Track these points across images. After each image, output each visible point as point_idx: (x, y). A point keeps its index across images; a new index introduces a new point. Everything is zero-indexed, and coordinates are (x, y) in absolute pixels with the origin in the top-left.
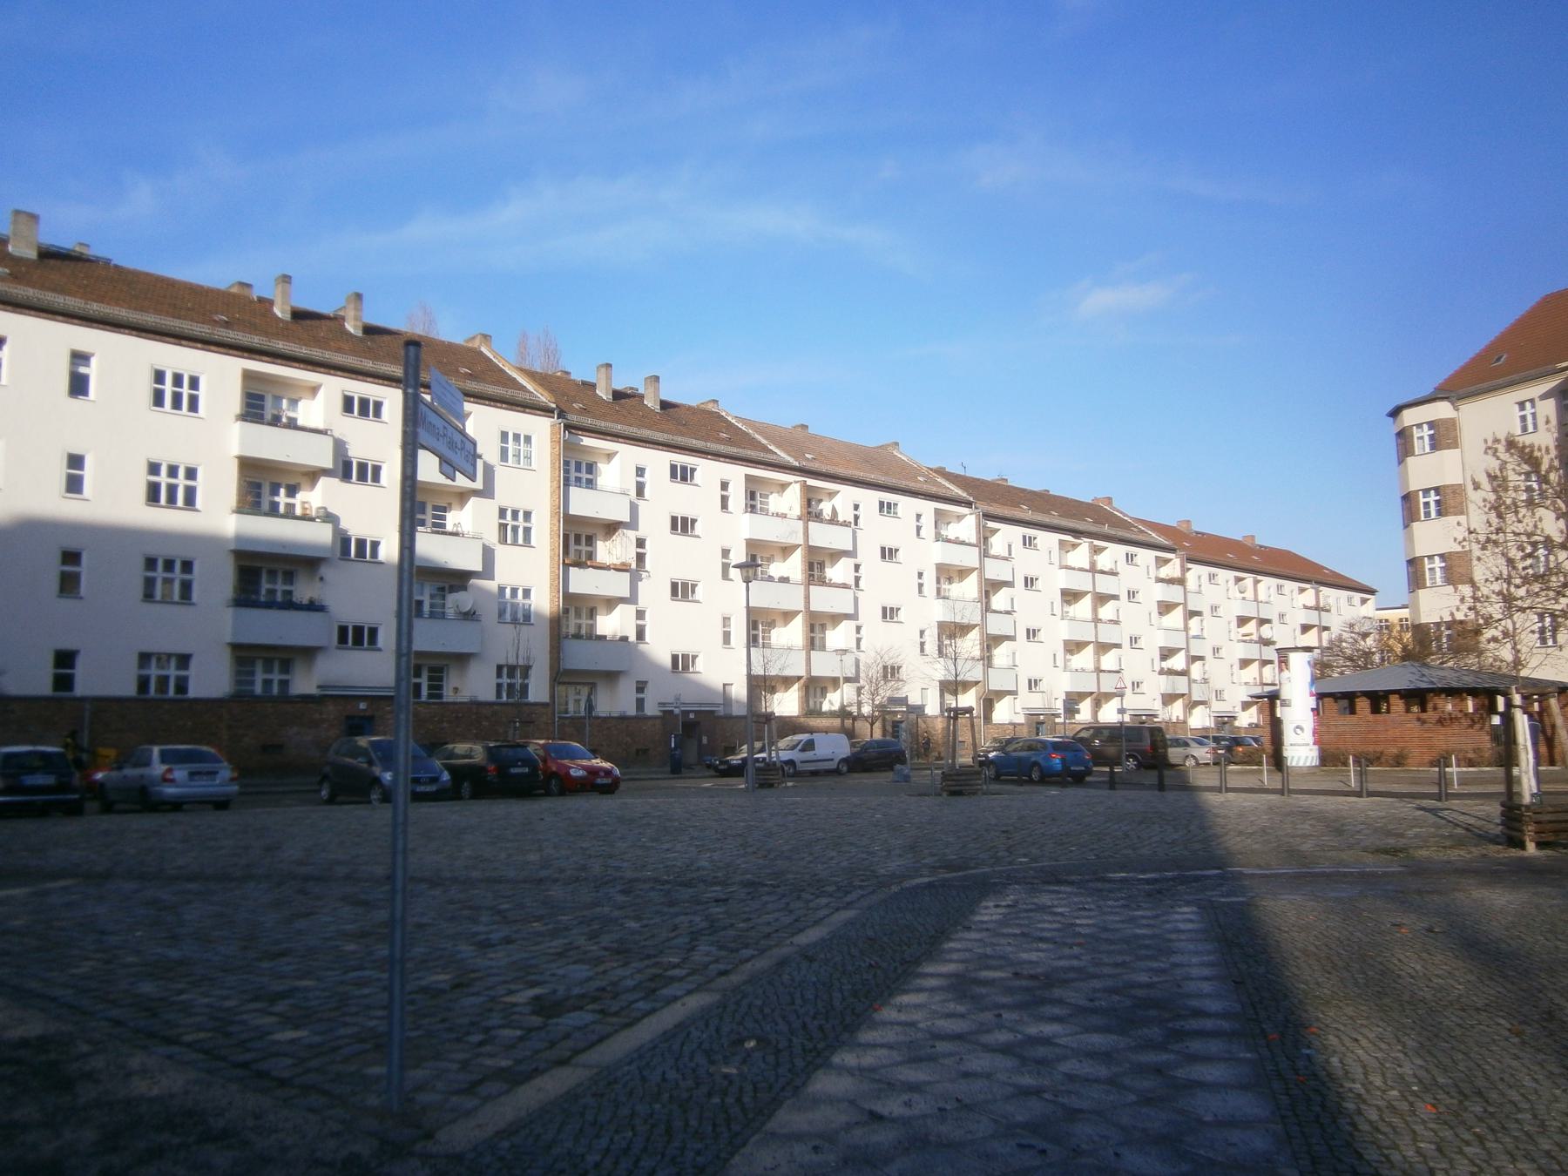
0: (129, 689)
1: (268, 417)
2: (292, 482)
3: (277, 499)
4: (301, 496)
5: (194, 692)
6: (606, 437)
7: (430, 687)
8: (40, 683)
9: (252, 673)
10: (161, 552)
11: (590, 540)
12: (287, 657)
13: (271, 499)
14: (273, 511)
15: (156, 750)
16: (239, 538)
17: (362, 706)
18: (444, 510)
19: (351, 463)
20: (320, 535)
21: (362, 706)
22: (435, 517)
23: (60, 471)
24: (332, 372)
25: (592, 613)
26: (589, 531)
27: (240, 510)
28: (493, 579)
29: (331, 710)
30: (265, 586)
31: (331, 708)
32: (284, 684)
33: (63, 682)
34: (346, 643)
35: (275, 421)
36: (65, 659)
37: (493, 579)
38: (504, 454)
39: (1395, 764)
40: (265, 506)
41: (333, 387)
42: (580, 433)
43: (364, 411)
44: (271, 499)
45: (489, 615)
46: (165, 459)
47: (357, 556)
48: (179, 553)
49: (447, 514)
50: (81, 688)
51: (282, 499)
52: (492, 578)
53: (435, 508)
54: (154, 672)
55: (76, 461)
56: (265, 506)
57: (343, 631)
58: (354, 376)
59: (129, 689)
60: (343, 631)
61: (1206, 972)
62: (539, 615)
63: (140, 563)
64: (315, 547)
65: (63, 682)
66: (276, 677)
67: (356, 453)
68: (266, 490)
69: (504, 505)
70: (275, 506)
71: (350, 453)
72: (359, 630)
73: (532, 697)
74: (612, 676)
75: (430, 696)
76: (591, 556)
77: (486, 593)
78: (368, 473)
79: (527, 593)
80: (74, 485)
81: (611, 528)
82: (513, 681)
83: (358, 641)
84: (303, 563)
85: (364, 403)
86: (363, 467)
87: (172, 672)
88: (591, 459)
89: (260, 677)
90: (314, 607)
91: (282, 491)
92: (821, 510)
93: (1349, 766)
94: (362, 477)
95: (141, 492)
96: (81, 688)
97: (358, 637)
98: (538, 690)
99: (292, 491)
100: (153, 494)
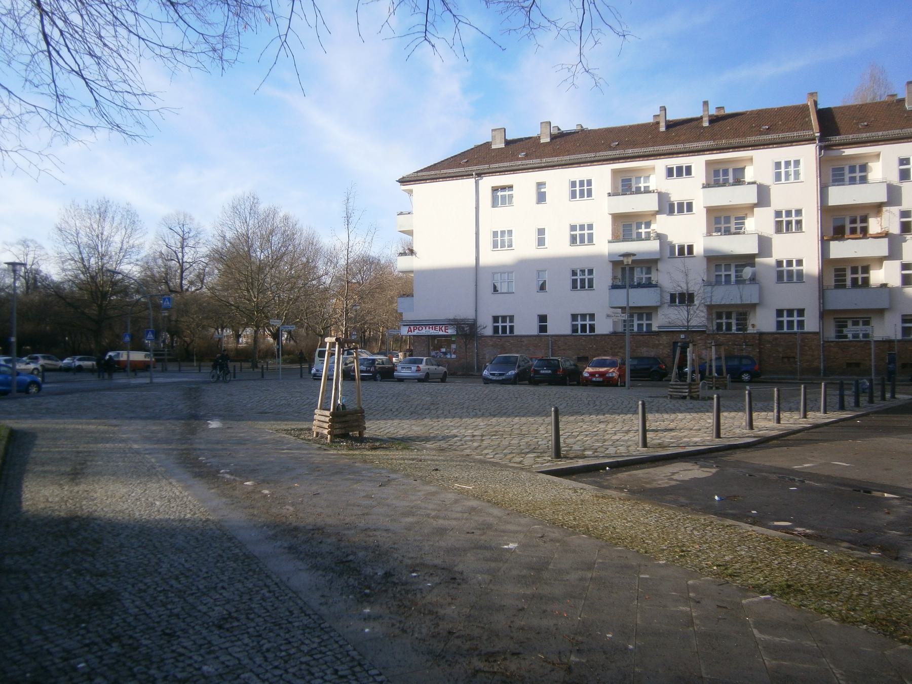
0: (567, 331)
1: (634, 189)
2: (648, 220)
3: (640, 231)
4: (653, 226)
6: (866, 145)
7: (737, 325)
8: (534, 330)
10: (578, 267)
11: (865, 219)
12: (647, 312)
13: (637, 231)
14: (639, 238)
16: (610, 255)
17: (682, 336)
18: (743, 218)
19: (674, 204)
20: (653, 246)
21: (682, 336)
22: (736, 224)
23: (534, 237)
24: (658, 157)
25: (866, 270)
26: (863, 213)
27: (709, 233)
28: (772, 257)
29: (664, 339)
31: (665, 338)
32: (649, 326)
33: (543, 329)
35: (638, 191)
36: (543, 319)
37: (772, 257)
38: (778, 177)
40: (634, 236)
41: (661, 165)
42: (841, 147)
43: (680, 174)
44: (637, 231)
46: (577, 222)
47: (688, 254)
48: (586, 266)
49: (745, 221)
50: (550, 331)
51: (643, 230)
53: (737, 218)
54: (579, 322)
55: (541, 232)
56: (634, 236)
58: (671, 156)
59: (567, 331)
62: (810, 277)
63: (569, 274)
64: (650, 253)
65: (543, 329)
66: (645, 322)
67: (675, 198)
68: (634, 227)
69: (779, 208)
70: (639, 234)
71: (672, 199)
74: (880, 312)
75: (738, 330)
77: (767, 266)
79: (800, 262)
80: (541, 242)
81: (877, 208)
84: (649, 263)
85: (680, 169)
86: (681, 205)
87: (795, 318)
88: (862, 162)
90: (649, 285)
91: (643, 226)
92: (286, 218)
94: (681, 211)
95: (568, 239)
96: (550, 331)
97: (685, 299)
98: (812, 324)
99: (648, 225)
100: (573, 240)
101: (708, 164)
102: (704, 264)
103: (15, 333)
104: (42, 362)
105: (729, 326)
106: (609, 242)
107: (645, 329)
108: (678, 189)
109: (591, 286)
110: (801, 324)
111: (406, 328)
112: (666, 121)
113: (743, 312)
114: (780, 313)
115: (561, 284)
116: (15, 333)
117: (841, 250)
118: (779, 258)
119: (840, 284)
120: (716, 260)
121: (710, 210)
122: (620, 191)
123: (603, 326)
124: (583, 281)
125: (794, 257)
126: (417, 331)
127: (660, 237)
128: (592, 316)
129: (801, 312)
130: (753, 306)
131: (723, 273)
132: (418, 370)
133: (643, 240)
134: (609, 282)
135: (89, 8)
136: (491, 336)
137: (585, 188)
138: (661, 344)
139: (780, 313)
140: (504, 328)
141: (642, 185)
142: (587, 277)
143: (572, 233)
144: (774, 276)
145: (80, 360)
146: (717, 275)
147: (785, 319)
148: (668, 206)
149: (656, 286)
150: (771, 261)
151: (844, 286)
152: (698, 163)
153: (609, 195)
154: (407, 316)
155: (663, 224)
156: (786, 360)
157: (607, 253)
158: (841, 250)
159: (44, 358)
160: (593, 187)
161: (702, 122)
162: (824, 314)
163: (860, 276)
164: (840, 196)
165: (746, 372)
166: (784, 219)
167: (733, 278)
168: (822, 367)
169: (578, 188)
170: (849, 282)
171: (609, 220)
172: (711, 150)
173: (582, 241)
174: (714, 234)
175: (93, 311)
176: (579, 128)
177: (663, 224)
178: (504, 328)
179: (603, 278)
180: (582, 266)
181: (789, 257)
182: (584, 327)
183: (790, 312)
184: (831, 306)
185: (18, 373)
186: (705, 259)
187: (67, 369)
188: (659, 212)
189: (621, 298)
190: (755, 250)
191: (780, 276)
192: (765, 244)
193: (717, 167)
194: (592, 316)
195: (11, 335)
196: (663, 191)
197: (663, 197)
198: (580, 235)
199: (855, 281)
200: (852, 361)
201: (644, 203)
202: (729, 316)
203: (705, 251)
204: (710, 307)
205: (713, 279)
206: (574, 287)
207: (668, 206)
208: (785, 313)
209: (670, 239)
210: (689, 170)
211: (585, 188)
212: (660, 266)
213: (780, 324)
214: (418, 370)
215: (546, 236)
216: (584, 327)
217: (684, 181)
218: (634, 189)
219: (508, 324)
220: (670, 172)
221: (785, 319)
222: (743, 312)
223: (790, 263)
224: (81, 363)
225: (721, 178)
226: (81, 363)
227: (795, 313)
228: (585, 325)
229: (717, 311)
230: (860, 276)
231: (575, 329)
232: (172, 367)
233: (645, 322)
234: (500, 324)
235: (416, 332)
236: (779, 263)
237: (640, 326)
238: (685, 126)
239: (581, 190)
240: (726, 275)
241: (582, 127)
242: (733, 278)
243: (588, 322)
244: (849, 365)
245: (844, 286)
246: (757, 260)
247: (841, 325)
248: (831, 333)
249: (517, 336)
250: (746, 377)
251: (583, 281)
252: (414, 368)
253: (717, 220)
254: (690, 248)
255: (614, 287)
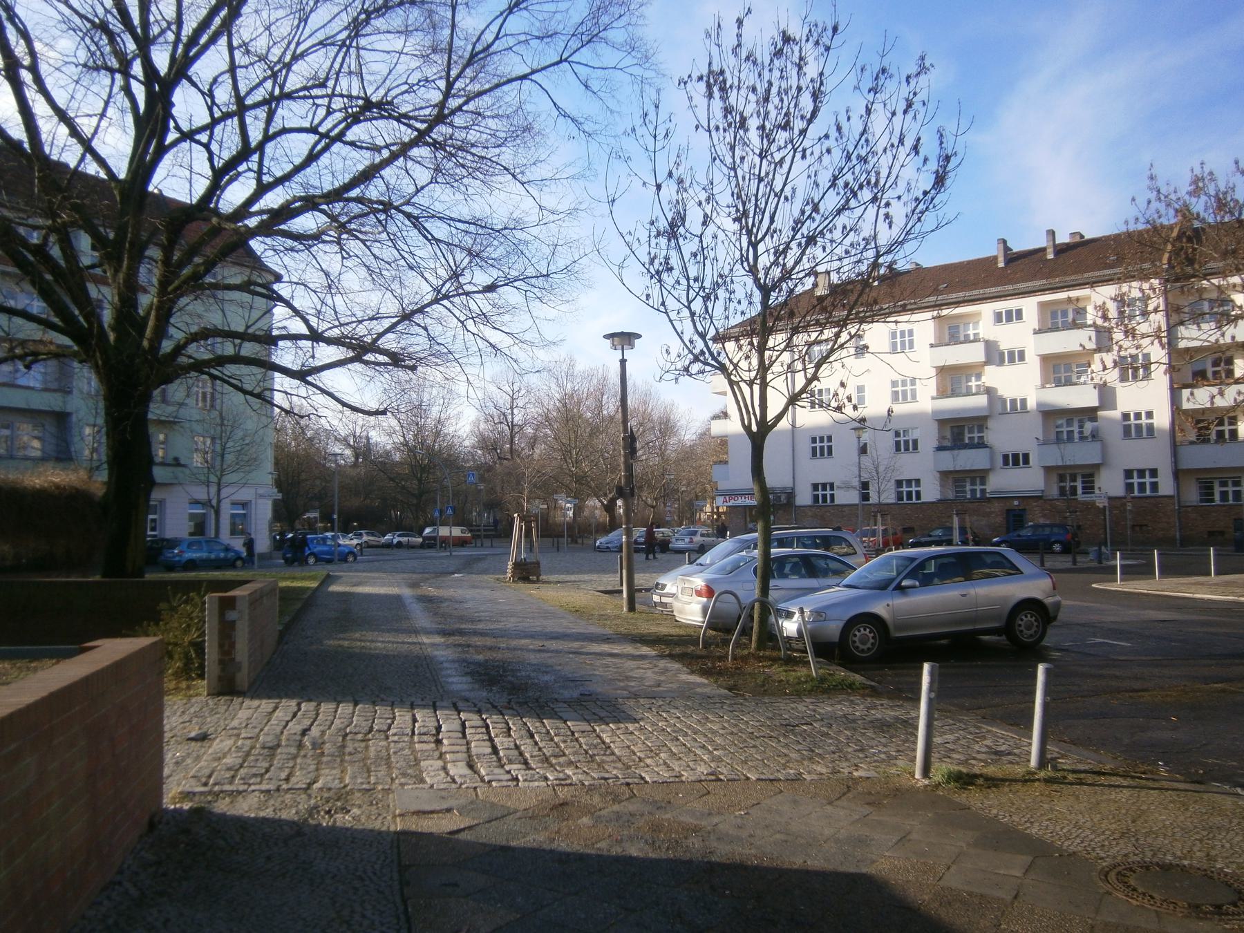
1: (962, 338)
4: (984, 379)
5: (837, 502)
7: (1084, 488)
9: (965, 487)
10: (817, 435)
11: (1230, 361)
12: (981, 476)
15: (150, 533)
16: (934, 412)
17: (1016, 503)
21: (1016, 503)
29: (997, 507)
30: (967, 435)
33: (865, 497)
34: (1008, 464)
35: (967, 340)
39: (813, 559)
41: (987, 310)
43: (1009, 319)
45: (1114, 437)
48: (825, 434)
51: (973, 383)
52: (1113, 407)
54: (905, 489)
57: (1006, 457)
60: (1006, 457)
61: (450, 680)
62: (1161, 431)
65: (865, 497)
66: (978, 488)
67: (1005, 346)
70: (969, 388)
72: (1016, 456)
73: (926, 498)
76: (1230, 373)
77: (1111, 421)
78: (1017, 356)
79: (1150, 415)
82: (974, 487)
83: (1016, 463)
84: (979, 421)
85: (1009, 313)
86: (1011, 354)
87: (1148, 480)
89: (968, 487)
90: (981, 445)
93: (1122, 566)
94: (1012, 360)
96: (837, 502)
97: (1017, 460)
98: (1166, 486)
99: (979, 377)
101: (1043, 306)
102: (1039, 420)
103: (336, 511)
104: (365, 538)
105: (1074, 489)
106: (933, 398)
107: (978, 496)
108: (1009, 337)
109: (830, 453)
110: (1154, 486)
111: (722, 499)
112: (1055, 246)
113: (1089, 475)
114: (1128, 474)
115: (882, 445)
116: (336, 511)
117: (1200, 398)
118: (1126, 410)
119: (1203, 439)
120: (1050, 414)
121: (1046, 359)
122: (947, 340)
123: (931, 492)
124: (822, 448)
125: (1143, 408)
126: (732, 501)
127: (989, 391)
128: (918, 482)
129: (1154, 472)
130: (1097, 467)
131: (1065, 429)
132: (691, 542)
133: (973, 395)
134: (935, 444)
135: (473, 150)
136: (810, 506)
137: (907, 339)
138: (993, 512)
139: (1128, 474)
140: (824, 497)
141: (971, 332)
142: (826, 444)
143: (894, 389)
144: (1120, 431)
145: (399, 536)
146: (1057, 432)
147: (1136, 480)
148: (994, 355)
149: (986, 446)
150: (1116, 414)
151: (1208, 441)
152: (1029, 305)
153: (932, 346)
154: (722, 485)
155: (993, 377)
156: (1137, 528)
157: (930, 411)
158: (1200, 398)
159: (367, 534)
160: (915, 338)
161: (1046, 255)
162: (1178, 474)
163: (1226, 428)
164: (1193, 336)
165: (1056, 542)
166: (900, 389)
167: (1076, 436)
168: (1178, 536)
169: (898, 340)
170: (1213, 436)
171: (1038, 359)
172: (1042, 290)
173: (905, 397)
174: (1048, 386)
175: (413, 485)
176: (914, 266)
177: (993, 377)
178: (824, 497)
179: (928, 438)
180: (822, 434)
181: (1137, 409)
182: (909, 494)
183: (1141, 473)
184: (1185, 465)
185: (339, 545)
186: (1040, 415)
187: (389, 546)
188: (988, 362)
189: (950, 461)
190: (1094, 402)
191: (1127, 431)
192: (1106, 395)
193: (1055, 308)
194: (918, 482)
195: (333, 513)
196: (991, 338)
197: (990, 347)
198: (903, 391)
199: (1220, 434)
200: (1216, 529)
201: (970, 354)
202: (1074, 479)
203: (1039, 405)
204: (1048, 470)
205: (1053, 437)
206: (814, 454)
207: (994, 355)
208: (1135, 474)
209: (1000, 393)
210: (1019, 313)
211: (907, 339)
212: (990, 424)
213: (1129, 487)
214: (691, 542)
215: (866, 394)
216: (909, 494)
217: (1015, 326)
218: (962, 338)
219: (828, 492)
220: (998, 317)
221: (1136, 480)
222: (1089, 475)
223: (1138, 416)
224: (401, 539)
225: (1060, 320)
226: (401, 539)
227: (1135, 474)
228: (911, 492)
229: (1061, 473)
230: (1226, 428)
231: (900, 497)
232: (487, 542)
233: (978, 488)
234: (820, 493)
235: (731, 503)
236: (1126, 416)
237: (973, 491)
238: (1026, 260)
239: (902, 344)
240: (1068, 432)
241: (1082, 237)
242: (1076, 436)
243: (914, 489)
244: (1211, 533)
245: (1208, 441)
246: (1100, 413)
247: (1206, 490)
248: (1192, 495)
249: (838, 505)
250: (1057, 547)
251: (822, 448)
252: (687, 540)
253: (1056, 369)
254: (1024, 401)
255: (940, 448)
